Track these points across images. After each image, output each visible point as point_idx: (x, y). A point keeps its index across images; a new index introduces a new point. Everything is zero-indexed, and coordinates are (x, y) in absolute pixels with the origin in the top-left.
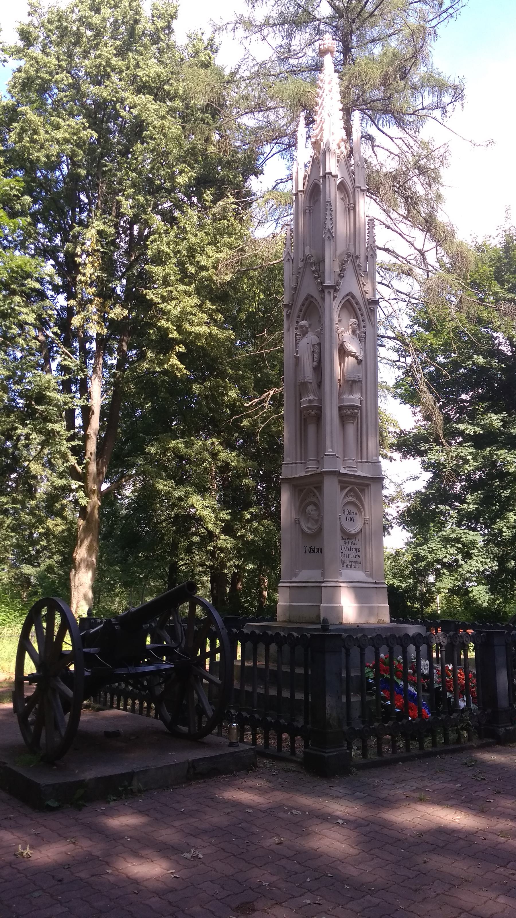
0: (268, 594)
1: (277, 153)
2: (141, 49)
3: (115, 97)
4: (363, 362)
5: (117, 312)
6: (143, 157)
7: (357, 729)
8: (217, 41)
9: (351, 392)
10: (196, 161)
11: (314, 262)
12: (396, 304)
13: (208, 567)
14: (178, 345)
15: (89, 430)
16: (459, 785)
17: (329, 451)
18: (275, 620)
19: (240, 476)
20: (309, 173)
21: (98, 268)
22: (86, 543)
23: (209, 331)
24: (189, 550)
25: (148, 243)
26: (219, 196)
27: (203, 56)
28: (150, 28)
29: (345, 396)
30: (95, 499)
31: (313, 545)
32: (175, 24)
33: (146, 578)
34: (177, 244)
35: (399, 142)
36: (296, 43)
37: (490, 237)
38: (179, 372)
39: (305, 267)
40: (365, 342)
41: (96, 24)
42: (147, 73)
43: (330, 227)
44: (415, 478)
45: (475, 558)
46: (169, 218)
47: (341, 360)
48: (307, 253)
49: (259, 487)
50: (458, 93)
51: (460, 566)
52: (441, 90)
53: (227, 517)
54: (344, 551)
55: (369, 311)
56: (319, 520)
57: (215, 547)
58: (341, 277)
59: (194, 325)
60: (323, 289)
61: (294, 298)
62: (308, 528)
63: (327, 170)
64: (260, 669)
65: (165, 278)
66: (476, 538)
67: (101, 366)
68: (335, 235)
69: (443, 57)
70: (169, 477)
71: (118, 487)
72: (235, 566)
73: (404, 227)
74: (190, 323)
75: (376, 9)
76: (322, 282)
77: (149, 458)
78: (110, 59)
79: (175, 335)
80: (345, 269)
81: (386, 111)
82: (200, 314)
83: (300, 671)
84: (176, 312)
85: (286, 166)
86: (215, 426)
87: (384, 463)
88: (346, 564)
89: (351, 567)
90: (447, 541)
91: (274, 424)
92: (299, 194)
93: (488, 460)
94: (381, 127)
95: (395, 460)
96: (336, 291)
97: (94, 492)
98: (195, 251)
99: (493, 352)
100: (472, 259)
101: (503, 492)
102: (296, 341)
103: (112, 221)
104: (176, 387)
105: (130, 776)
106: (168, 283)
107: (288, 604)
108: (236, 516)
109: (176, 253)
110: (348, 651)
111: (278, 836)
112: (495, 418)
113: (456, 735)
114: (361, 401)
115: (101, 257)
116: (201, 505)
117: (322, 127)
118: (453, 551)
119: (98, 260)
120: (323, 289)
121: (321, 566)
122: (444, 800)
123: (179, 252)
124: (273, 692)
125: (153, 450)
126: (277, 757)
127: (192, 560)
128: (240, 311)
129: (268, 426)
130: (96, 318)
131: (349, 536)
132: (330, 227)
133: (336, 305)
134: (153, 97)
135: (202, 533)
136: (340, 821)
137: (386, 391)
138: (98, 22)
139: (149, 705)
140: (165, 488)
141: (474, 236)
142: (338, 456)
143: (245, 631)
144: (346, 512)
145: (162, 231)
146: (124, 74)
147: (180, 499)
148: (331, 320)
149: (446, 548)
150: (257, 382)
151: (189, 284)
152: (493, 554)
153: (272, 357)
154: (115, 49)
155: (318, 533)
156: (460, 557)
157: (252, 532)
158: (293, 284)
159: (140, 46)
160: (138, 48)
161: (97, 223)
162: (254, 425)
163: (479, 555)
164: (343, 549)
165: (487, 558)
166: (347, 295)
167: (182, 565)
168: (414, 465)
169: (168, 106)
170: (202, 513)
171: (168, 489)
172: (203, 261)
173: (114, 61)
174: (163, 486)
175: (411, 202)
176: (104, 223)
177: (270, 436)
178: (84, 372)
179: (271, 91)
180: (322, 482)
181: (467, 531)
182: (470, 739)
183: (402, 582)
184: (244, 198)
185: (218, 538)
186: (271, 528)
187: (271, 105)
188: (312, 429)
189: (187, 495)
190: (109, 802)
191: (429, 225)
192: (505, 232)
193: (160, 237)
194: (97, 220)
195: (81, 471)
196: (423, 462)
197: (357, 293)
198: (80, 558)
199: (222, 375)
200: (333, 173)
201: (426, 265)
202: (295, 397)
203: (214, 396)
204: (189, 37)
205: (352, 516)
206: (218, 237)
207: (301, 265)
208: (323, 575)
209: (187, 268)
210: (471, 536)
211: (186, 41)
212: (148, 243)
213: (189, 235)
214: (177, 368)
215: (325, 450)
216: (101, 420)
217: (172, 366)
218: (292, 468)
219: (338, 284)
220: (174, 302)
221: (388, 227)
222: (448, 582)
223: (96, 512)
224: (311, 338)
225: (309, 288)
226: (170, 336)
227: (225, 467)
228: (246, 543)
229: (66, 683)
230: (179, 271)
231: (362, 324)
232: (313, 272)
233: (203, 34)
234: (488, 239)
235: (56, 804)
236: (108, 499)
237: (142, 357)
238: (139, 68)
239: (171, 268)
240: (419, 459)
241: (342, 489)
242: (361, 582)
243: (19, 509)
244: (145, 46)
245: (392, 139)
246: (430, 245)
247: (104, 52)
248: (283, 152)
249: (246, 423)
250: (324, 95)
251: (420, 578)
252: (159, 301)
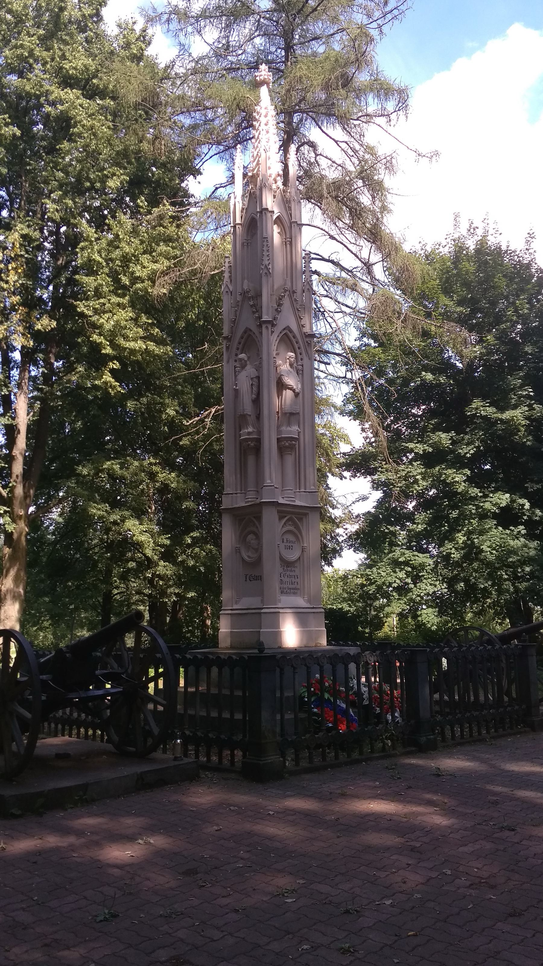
0: (212, 622)
1: (216, 154)
2: (67, 38)
3: (39, 91)
4: (301, 395)
5: (45, 323)
6: (71, 153)
7: (290, 739)
8: (150, 31)
9: (289, 424)
10: (129, 163)
11: (252, 297)
12: (340, 321)
13: (147, 595)
14: (112, 361)
15: (14, 451)
16: (378, 783)
17: (268, 482)
18: (218, 647)
19: (180, 497)
20: (246, 206)
21: (22, 275)
22: (12, 573)
23: (145, 347)
24: (124, 577)
25: (77, 250)
26: (154, 202)
27: (134, 48)
28: (76, 14)
29: (284, 428)
30: (22, 526)
31: (253, 572)
32: (104, 12)
33: (76, 609)
34: (109, 252)
35: (343, 145)
36: (234, 38)
37: (439, 245)
38: (113, 390)
39: (243, 300)
40: (302, 374)
41: (17, 11)
42: (74, 65)
43: (267, 263)
44: (364, 498)
45: (424, 581)
46: (99, 223)
47: (280, 394)
48: (245, 287)
49: (201, 508)
50: (403, 103)
51: (410, 590)
52: (386, 94)
53: (168, 542)
54: (283, 578)
55: (306, 344)
56: (258, 549)
57: (153, 575)
58: (278, 311)
59: (129, 341)
60: (261, 324)
61: (232, 330)
62: (249, 557)
63: (264, 206)
64: (202, 694)
65: (97, 290)
66: (425, 560)
67: (27, 381)
68: (273, 271)
69: (389, 59)
70: (104, 500)
71: (44, 509)
72: (175, 594)
73: (350, 236)
74: (124, 338)
75: (319, 5)
76: (260, 317)
77: (80, 479)
78: (32, 50)
79: (108, 350)
80: (282, 304)
81: (329, 115)
82: (135, 329)
83: (239, 693)
84: (108, 326)
85: (225, 167)
86: (153, 443)
87: (332, 481)
90: (396, 564)
91: (216, 441)
92: (237, 226)
93: (437, 478)
94: (324, 129)
95: (346, 478)
96: (273, 325)
97: (20, 517)
98: (130, 261)
99: (445, 367)
100: (419, 272)
101: (451, 513)
102: (235, 372)
103: (38, 224)
104: (107, 402)
105: (85, 787)
106: (101, 294)
107: (229, 630)
108: (177, 540)
109: (109, 260)
110: (282, 670)
111: (217, 825)
112: (443, 435)
113: (381, 744)
114: (299, 433)
115: (26, 263)
116: (137, 529)
117: (258, 161)
118: (402, 575)
119: (23, 266)
120: (261, 324)
121: (261, 593)
123: (111, 260)
124: (214, 714)
125: (85, 472)
126: (218, 769)
127: (127, 589)
128: (177, 319)
129: (211, 444)
130: (20, 329)
131: (287, 564)
132: (267, 263)
133: (274, 339)
134: (80, 92)
135: (139, 558)
136: (271, 813)
137: (333, 409)
138: (20, 9)
139: (95, 732)
140: (99, 512)
141: (423, 243)
142: (277, 484)
143: (188, 656)
144: (285, 541)
145: (93, 239)
146: (48, 66)
147: (115, 523)
148: (269, 354)
149: (395, 572)
150: (197, 397)
151: (123, 296)
152: (442, 576)
153: (212, 372)
154: (39, 39)
155: (258, 563)
156: (409, 580)
157: (193, 558)
158: (232, 317)
159: (66, 35)
160: (64, 37)
161: (19, 226)
162: (194, 443)
163: (429, 578)
165: (436, 581)
166: (284, 329)
167: (116, 594)
168: (362, 484)
169: (98, 104)
170: (139, 538)
171: (102, 513)
172: (139, 272)
173: (37, 52)
174: (97, 510)
175: (357, 212)
176: (29, 226)
177: (211, 454)
178: (9, 387)
179: (209, 92)
180: (261, 512)
181: (416, 553)
182: (393, 747)
183: (350, 606)
184: (180, 198)
185: (157, 565)
186: (214, 552)
187: (208, 104)
188: (251, 460)
189: (123, 521)
190: (66, 810)
191: (375, 235)
192: (454, 241)
193: (91, 244)
194: (20, 222)
195: (6, 495)
196: (373, 481)
197: (294, 327)
198: (5, 589)
199: (159, 390)
200: (270, 209)
201: (373, 278)
202: (235, 429)
203: (152, 414)
204: (119, 26)
205: (290, 544)
206: (153, 244)
207: (239, 298)
209: (120, 279)
210: (421, 558)
211: (116, 31)
212: (77, 250)
213: (123, 244)
214: (111, 386)
215: (263, 481)
216: (27, 438)
217: (106, 383)
218: (233, 498)
219: (275, 319)
220: (107, 315)
221: (332, 237)
222: (398, 606)
223: (23, 539)
224: (250, 370)
225: (247, 321)
226: (103, 351)
227: (165, 489)
228: (187, 569)
229: (23, 708)
230: (111, 281)
231: (300, 357)
232: (252, 306)
233: (134, 23)
234: (437, 247)
235: (19, 812)
236: (34, 523)
237: (69, 368)
238: (65, 59)
239: (103, 280)
240: (369, 478)
241: (281, 518)
244: (71, 35)
245: (336, 142)
246: (376, 257)
247: (26, 41)
248: (222, 154)
249: (185, 442)
250: (260, 128)
251: (369, 602)
252: (90, 313)
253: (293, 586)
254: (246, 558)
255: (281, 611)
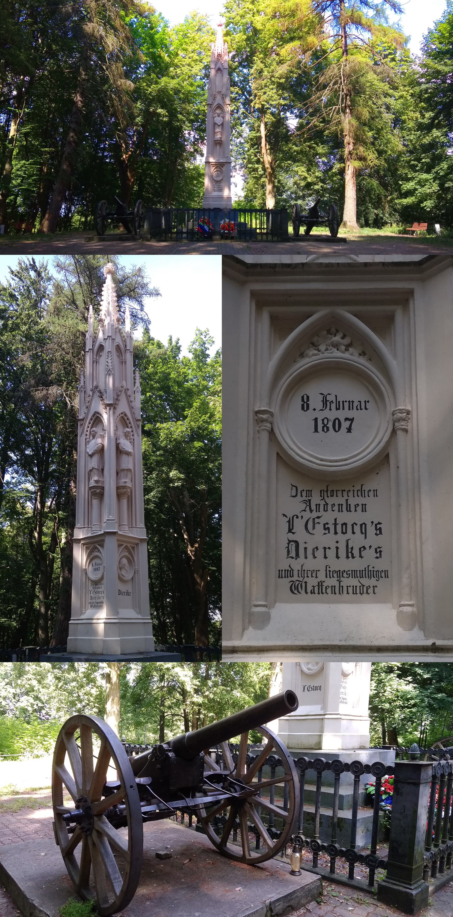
54: (300, 535)
62: (309, 669)
88: (312, 582)
89: (338, 591)
122: (155, 246)
144: (316, 402)
164: (299, 525)
205: (342, 414)
208: (324, 708)
243: (5, 593)
253: (356, 564)
254: (305, 669)
255: (343, 717)
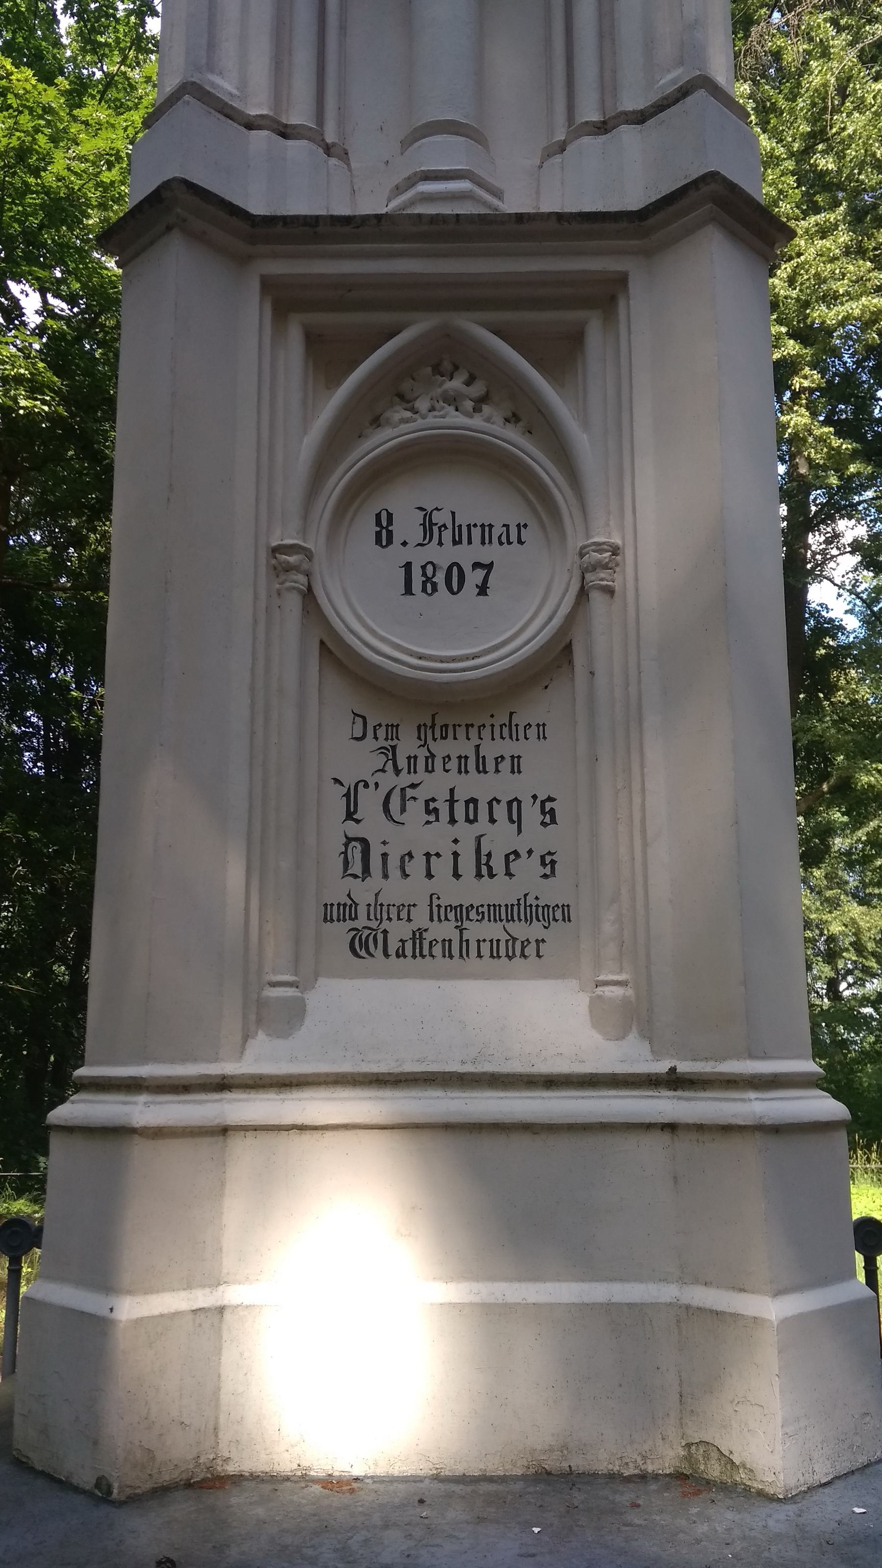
54: (372, 824)
88: (399, 931)
89: (458, 950)
107: (129, 1309)
144: (407, 526)
164: (369, 803)
205: (466, 555)
242: (551, 1082)
253: (498, 891)
255: (143, 1111)
